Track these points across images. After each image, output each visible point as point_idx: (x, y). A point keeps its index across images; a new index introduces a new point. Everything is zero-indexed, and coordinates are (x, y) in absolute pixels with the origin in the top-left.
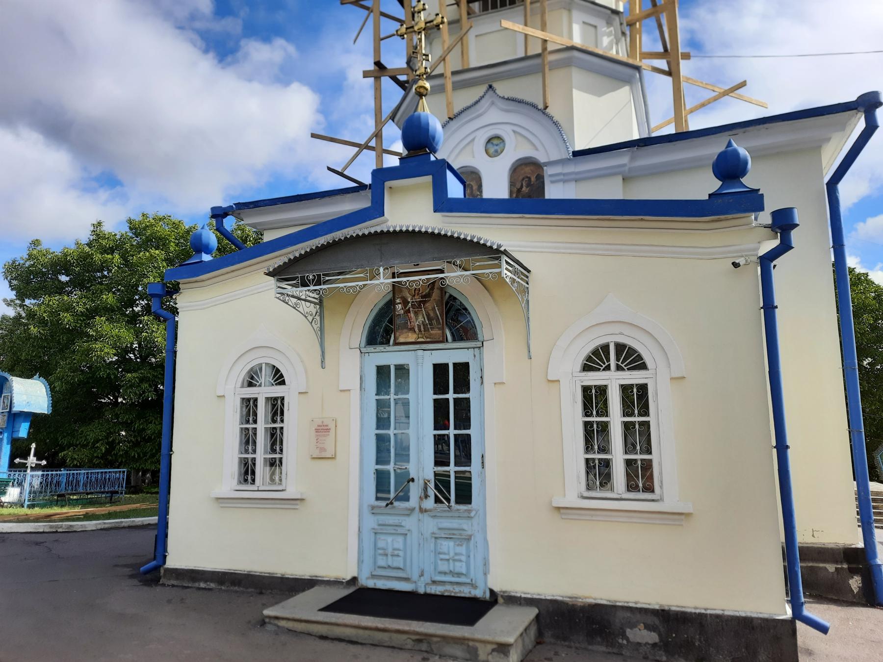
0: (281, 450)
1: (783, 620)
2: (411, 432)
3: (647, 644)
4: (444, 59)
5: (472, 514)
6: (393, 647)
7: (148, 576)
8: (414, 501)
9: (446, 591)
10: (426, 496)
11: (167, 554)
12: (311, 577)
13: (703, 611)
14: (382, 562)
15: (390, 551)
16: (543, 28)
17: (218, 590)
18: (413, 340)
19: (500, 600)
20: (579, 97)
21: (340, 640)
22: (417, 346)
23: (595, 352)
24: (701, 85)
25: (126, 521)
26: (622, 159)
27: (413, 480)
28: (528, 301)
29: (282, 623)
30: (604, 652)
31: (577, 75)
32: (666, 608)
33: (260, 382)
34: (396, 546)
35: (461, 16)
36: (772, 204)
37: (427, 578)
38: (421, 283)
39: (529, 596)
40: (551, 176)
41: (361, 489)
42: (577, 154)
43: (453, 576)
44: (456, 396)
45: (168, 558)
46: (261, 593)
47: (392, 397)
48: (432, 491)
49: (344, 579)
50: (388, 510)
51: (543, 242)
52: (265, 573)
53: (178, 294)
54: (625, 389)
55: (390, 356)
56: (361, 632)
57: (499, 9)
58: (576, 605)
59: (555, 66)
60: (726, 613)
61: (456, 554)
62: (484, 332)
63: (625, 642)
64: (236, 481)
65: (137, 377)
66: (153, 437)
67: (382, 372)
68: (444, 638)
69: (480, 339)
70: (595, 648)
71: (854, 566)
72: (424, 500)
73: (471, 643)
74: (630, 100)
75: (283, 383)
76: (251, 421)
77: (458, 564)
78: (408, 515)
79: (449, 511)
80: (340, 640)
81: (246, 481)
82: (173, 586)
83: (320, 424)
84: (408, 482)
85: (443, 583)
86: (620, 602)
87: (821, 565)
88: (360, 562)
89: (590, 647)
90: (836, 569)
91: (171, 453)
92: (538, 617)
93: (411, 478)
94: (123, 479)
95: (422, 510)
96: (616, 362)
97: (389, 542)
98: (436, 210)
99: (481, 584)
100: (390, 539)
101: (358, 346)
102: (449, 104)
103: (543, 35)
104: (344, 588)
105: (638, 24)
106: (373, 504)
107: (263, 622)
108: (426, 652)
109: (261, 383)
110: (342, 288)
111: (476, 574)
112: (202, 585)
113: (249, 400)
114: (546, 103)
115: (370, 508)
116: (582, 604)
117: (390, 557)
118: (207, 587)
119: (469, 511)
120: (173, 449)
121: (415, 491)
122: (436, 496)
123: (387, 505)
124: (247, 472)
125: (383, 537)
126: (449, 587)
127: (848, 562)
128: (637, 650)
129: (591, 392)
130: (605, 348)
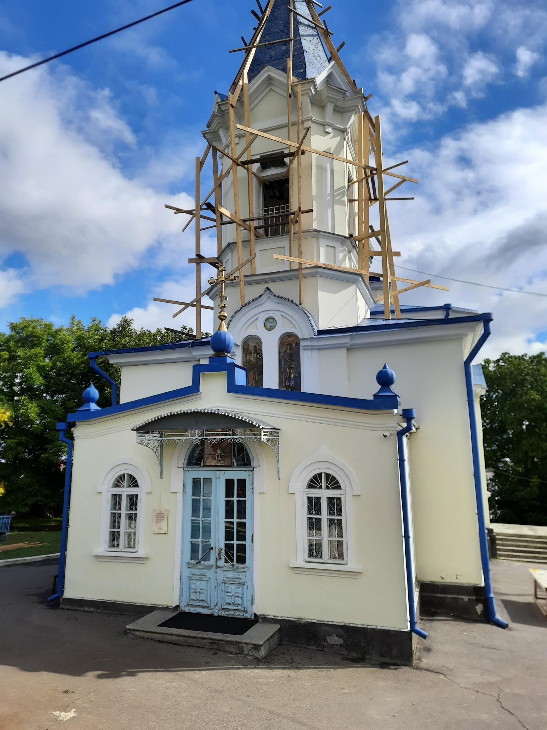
0: (135, 527)
1: (405, 632)
2: (212, 519)
3: (337, 644)
4: (239, 270)
5: (246, 570)
6: (199, 647)
7: (52, 603)
8: (212, 561)
9: (230, 614)
10: (220, 559)
11: (64, 589)
12: (151, 605)
13: (366, 627)
14: (193, 597)
15: (198, 590)
16: (300, 257)
17: (96, 612)
18: (214, 464)
19: (260, 620)
20: (321, 295)
21: (169, 643)
22: (216, 468)
23: (315, 477)
24: (402, 280)
25: (20, 560)
26: (345, 339)
27: (212, 548)
28: (279, 446)
29: (137, 633)
30: (315, 649)
31: (320, 282)
32: (348, 625)
33: (123, 484)
34: (202, 587)
35: (250, 238)
36: (404, 405)
37: (219, 607)
38: (218, 440)
39: (276, 618)
40: (303, 346)
41: (182, 553)
42: (320, 332)
43: (234, 606)
44: (238, 499)
45: (65, 592)
46: (122, 615)
47: (202, 498)
48: (223, 557)
49: (171, 607)
50: (197, 566)
51: (287, 412)
52: (124, 602)
53: (74, 428)
54: (330, 500)
55: (201, 473)
56: (181, 638)
57: (275, 236)
58: (300, 623)
59: (306, 276)
60: (378, 628)
61: (236, 593)
62: (254, 462)
63: (326, 644)
64: (107, 545)
65: (15, 442)
66: (24, 488)
67: (196, 482)
68: (226, 641)
69: (252, 465)
70: (311, 647)
71: (478, 598)
72: (219, 560)
73: (240, 645)
74: (356, 294)
75: (137, 486)
76: (117, 508)
77: (237, 599)
78: (209, 569)
79: (232, 568)
80: (169, 643)
81: (114, 546)
82: (68, 609)
83: (159, 512)
84: (210, 550)
85: (228, 610)
86: (324, 621)
87: (461, 597)
88: (181, 596)
89: (308, 647)
90: (469, 599)
91: (68, 526)
92: (280, 629)
93: (211, 547)
94: (8, 523)
95: (217, 567)
96: (326, 484)
97: (198, 585)
98: (228, 391)
99: (249, 611)
100: (198, 583)
101: (182, 466)
102: (242, 297)
103: (299, 260)
104: (171, 612)
105: (363, 241)
106: (189, 562)
107: (126, 632)
108: (216, 649)
109: (124, 485)
110: (174, 440)
111: (247, 605)
112: (86, 609)
113: (116, 495)
114: (301, 302)
115: (187, 565)
116: (304, 623)
117: (198, 594)
118: (89, 610)
119: (244, 568)
120: (70, 524)
121: (213, 555)
122: (225, 559)
123: (197, 563)
124: (114, 537)
125: (194, 582)
126: (231, 612)
127: (476, 595)
128: (332, 648)
129: (312, 500)
130: (320, 475)
